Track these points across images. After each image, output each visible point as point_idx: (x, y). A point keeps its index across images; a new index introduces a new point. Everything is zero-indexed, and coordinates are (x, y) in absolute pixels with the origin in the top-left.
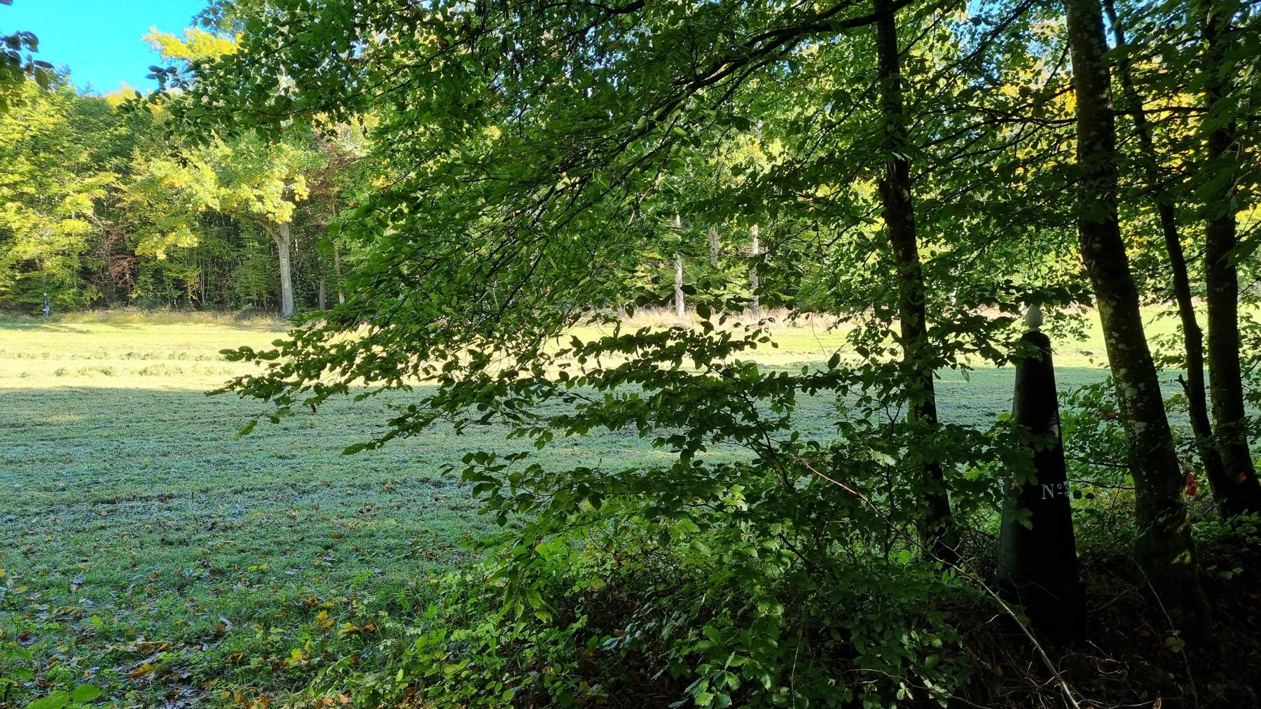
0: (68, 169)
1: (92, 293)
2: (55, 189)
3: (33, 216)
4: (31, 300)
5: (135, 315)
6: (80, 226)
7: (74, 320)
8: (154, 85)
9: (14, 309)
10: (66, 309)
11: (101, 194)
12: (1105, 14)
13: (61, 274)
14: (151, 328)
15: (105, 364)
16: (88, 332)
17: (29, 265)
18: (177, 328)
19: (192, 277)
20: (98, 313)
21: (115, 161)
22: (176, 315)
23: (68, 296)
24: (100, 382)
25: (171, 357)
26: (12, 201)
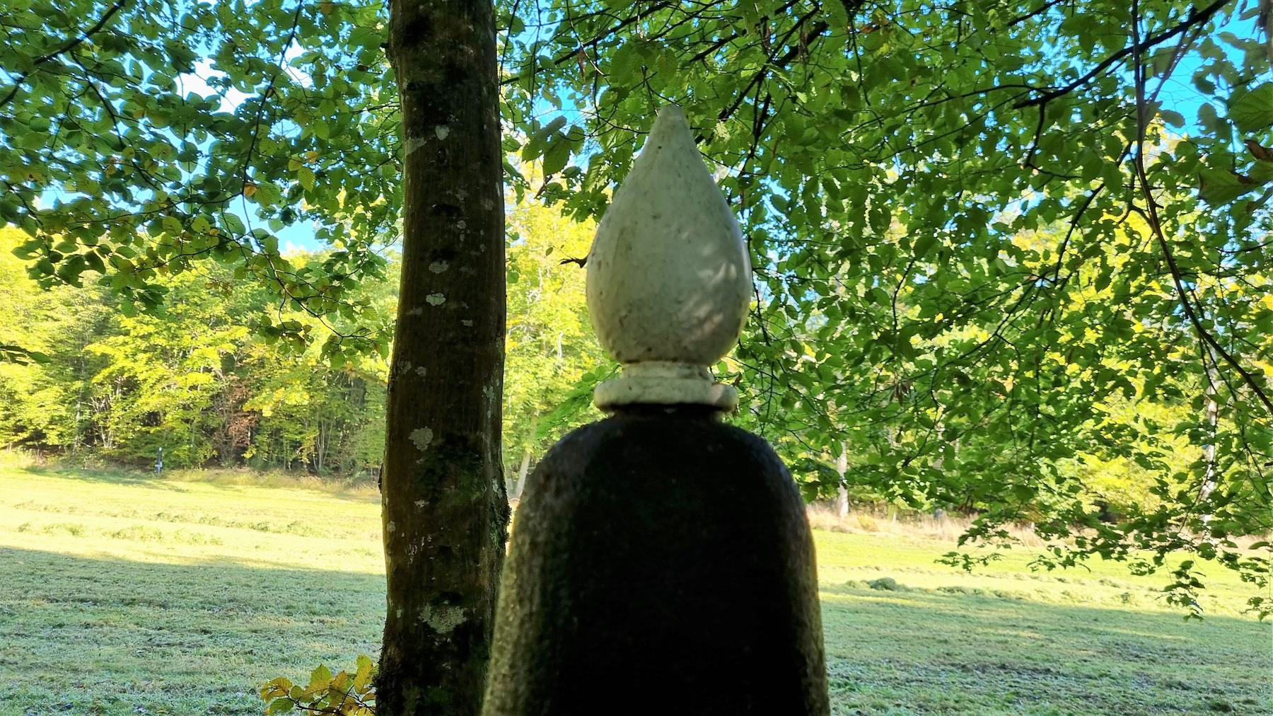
0: (203, 321)
1: (207, 451)
2: (186, 341)
3: (161, 368)
4: (148, 455)
5: (245, 474)
6: (203, 379)
7: (181, 478)
8: (558, 343)
9: (131, 463)
10: (178, 465)
11: (230, 348)
12: (1254, 85)
13: (181, 428)
14: (253, 491)
15: (74, 520)
16: (182, 491)
17: (153, 418)
18: (281, 493)
19: (309, 438)
20: (207, 473)
21: (250, 315)
22: (287, 479)
23: (183, 451)
24: (60, 544)
25: (202, 520)
26: (145, 351)
